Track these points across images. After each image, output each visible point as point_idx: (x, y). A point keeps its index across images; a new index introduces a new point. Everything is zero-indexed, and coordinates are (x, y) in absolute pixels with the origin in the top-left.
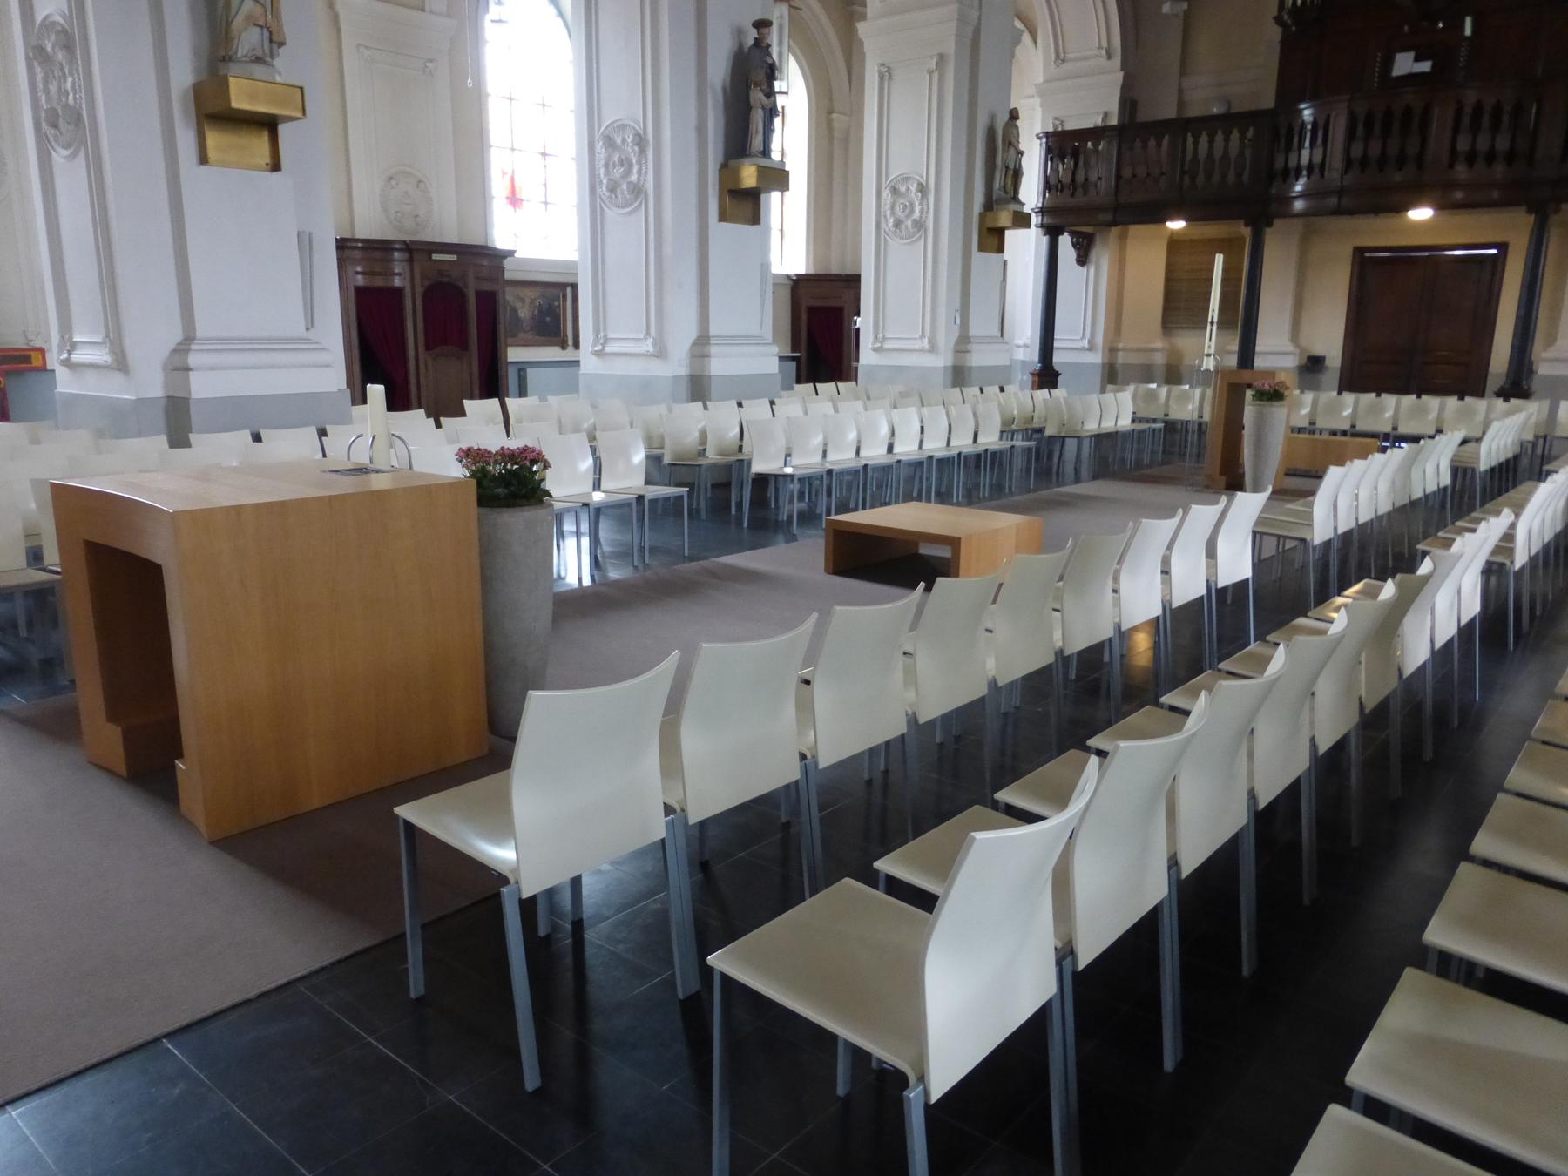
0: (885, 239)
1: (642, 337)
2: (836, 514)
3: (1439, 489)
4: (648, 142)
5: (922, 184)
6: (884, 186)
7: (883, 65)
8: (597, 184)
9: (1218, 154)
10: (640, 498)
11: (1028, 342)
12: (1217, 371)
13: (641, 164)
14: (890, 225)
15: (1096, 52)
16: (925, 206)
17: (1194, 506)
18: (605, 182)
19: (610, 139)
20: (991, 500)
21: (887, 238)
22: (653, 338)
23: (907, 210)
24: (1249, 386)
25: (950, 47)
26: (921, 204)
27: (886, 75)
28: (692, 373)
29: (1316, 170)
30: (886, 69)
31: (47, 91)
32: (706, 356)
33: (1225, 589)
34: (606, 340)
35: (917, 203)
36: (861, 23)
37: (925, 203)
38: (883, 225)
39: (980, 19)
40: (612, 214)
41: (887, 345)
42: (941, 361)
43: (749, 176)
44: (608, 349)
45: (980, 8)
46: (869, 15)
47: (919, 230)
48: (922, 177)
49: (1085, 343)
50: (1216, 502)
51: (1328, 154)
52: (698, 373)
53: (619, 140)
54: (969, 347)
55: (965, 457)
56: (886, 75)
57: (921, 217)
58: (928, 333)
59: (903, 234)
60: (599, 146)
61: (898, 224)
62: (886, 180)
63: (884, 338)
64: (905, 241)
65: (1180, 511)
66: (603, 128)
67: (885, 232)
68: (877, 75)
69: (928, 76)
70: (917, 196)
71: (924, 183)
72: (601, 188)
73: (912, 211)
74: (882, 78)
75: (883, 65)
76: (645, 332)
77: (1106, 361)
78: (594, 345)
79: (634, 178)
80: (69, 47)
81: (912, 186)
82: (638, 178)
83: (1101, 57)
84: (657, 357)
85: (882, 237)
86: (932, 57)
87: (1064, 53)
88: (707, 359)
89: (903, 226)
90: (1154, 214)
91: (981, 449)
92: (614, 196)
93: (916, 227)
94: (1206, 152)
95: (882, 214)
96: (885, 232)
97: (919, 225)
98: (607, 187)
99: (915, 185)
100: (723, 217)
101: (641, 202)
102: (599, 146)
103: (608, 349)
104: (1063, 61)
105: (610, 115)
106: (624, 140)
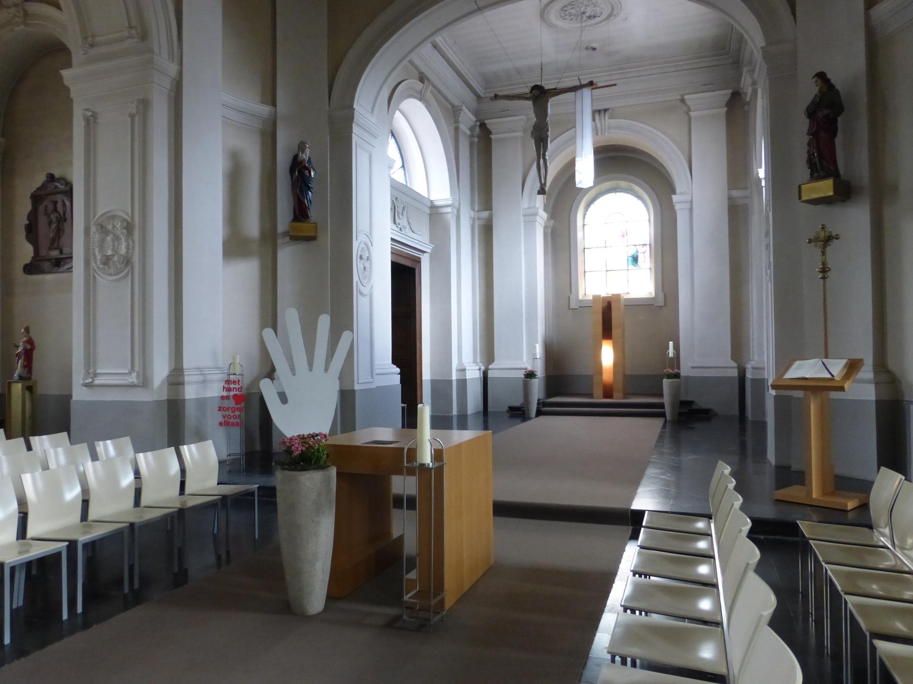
7: (87, 110)
12: (466, 379)
18: (99, 257)
19: (102, 226)
21: (96, 275)
22: (137, 372)
26: (127, 241)
31: (102, 247)
34: (96, 375)
36: (63, 70)
38: (93, 264)
39: (180, 73)
41: (98, 381)
57: (127, 252)
61: (107, 260)
66: (96, 218)
69: (129, 119)
70: (122, 233)
75: (87, 110)
76: (130, 368)
80: (129, 228)
83: (132, 37)
85: (91, 274)
88: (181, 386)
89: (111, 262)
91: (98, 532)
95: (91, 252)
101: (129, 271)
106: (114, 227)
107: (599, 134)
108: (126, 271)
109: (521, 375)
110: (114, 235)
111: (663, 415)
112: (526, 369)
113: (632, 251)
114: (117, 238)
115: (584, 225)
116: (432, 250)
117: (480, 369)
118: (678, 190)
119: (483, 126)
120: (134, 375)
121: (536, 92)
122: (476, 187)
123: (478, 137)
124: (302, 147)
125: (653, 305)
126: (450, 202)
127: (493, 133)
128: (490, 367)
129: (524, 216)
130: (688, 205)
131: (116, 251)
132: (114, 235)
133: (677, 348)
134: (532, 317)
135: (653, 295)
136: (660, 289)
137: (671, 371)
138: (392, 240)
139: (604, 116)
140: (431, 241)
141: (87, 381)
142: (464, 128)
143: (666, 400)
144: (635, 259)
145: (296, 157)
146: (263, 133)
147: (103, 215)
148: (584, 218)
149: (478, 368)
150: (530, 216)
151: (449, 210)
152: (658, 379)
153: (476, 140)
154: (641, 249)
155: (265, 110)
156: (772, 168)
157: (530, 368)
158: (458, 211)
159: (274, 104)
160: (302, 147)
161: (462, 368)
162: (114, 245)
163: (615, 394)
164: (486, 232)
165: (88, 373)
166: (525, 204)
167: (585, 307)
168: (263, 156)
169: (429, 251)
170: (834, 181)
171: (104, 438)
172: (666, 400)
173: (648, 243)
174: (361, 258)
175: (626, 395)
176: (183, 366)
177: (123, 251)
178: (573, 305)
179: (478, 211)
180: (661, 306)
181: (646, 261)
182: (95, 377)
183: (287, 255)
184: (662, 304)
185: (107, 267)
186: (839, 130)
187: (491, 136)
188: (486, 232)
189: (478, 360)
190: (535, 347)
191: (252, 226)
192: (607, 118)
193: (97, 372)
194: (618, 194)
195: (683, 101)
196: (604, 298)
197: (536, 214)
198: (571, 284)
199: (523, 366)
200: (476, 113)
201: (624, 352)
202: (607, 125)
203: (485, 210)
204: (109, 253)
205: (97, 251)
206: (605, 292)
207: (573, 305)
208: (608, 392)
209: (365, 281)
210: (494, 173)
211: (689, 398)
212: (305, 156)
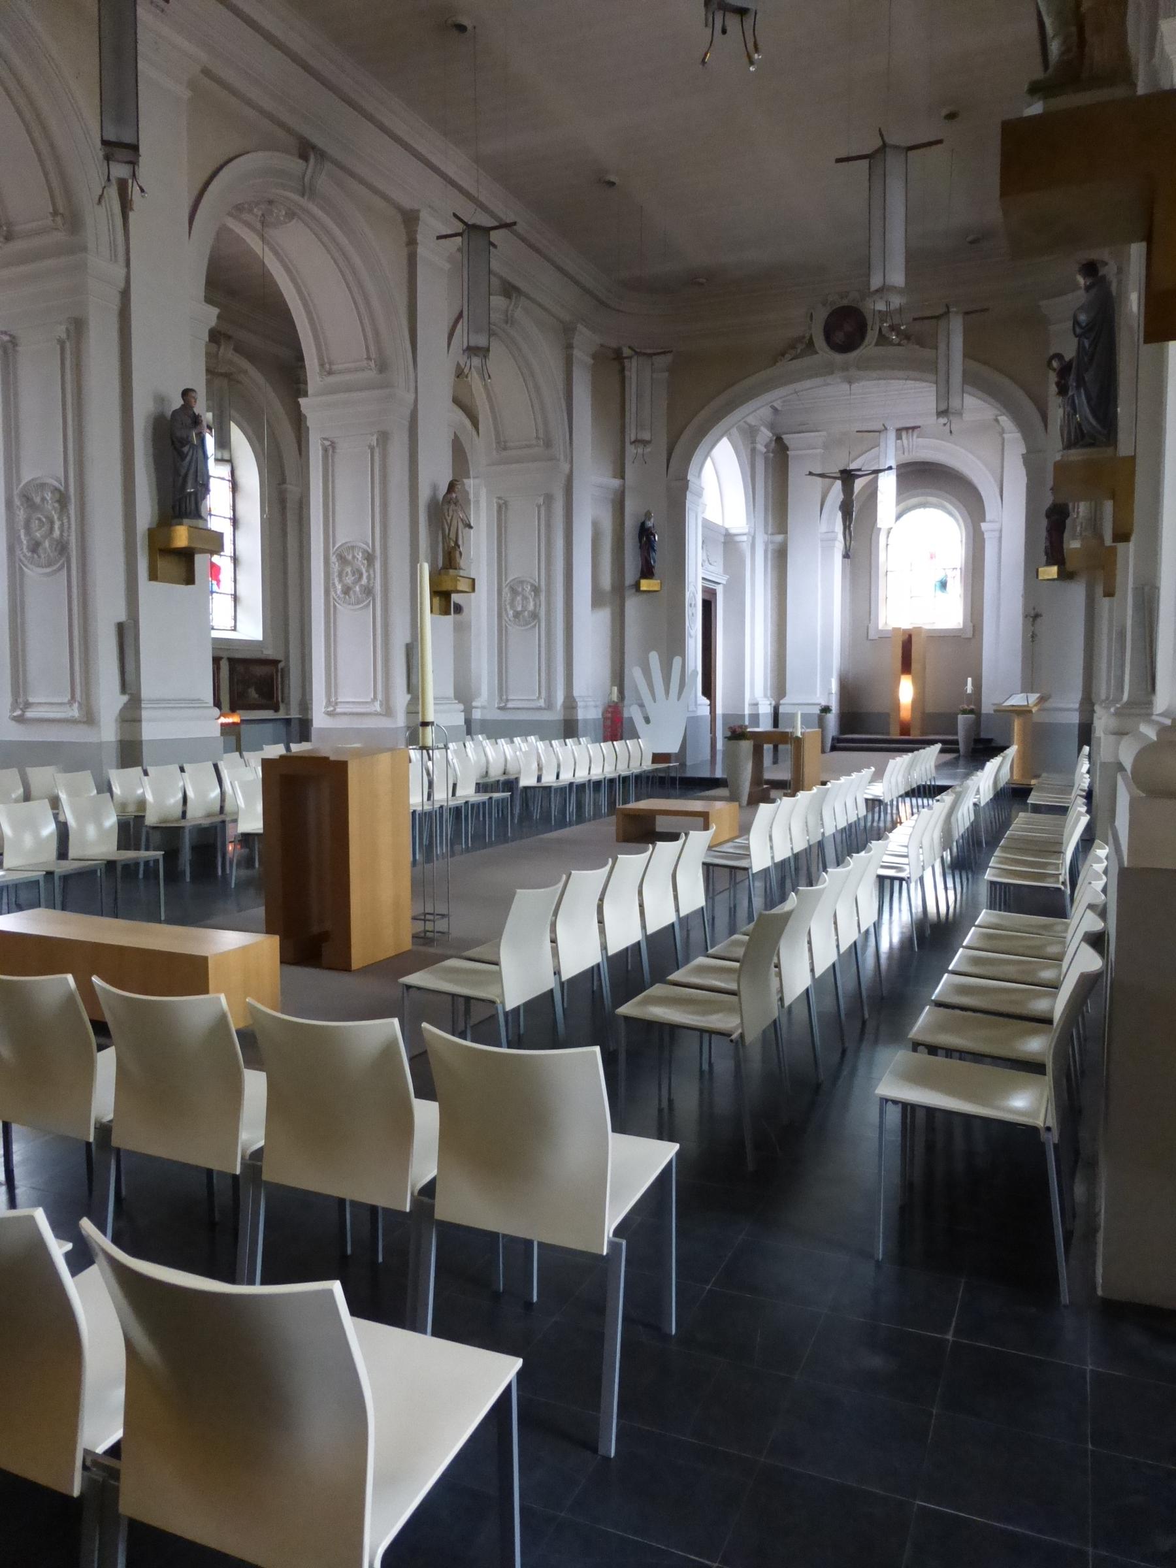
0: (506, 627)
1: (369, 700)
2: (956, 734)
3: (859, 819)
4: (69, 498)
6: (504, 585)
10: (49, 874)
11: (485, 704)
13: (62, 521)
14: (339, 592)
15: (534, 442)
16: (371, 572)
17: (518, 891)
20: (608, 816)
26: (534, 600)
27: (330, 449)
28: (566, 718)
30: (329, 443)
32: (139, 720)
33: (516, 1010)
34: (28, 705)
40: (33, 573)
41: (510, 705)
43: (181, 536)
46: (310, 392)
47: (534, 619)
48: (535, 580)
49: (542, 703)
50: (645, 851)
52: (569, 718)
53: (38, 500)
55: (473, 805)
56: (330, 449)
57: (61, 535)
58: (380, 697)
59: (353, 599)
60: (333, 559)
62: (333, 547)
63: (507, 700)
64: (523, 628)
65: (610, 860)
67: (334, 599)
68: (320, 448)
70: (363, 564)
71: (370, 551)
72: (22, 549)
73: (52, 529)
74: (325, 450)
77: (119, 738)
78: (13, 710)
79: (364, 581)
81: (358, 554)
84: (84, 723)
85: (332, 604)
86: (373, 435)
91: (460, 802)
96: (334, 599)
97: (368, 591)
98: (28, 547)
100: (153, 576)
102: (333, 559)
105: (27, 475)
106: (43, 499)
107: (906, 454)
108: (533, 624)
109: (817, 710)
110: (523, 596)
111: (957, 751)
112: (819, 704)
113: (940, 577)
114: (525, 598)
115: (887, 545)
116: (727, 581)
117: (771, 704)
118: (988, 517)
119: (779, 440)
120: (76, 705)
121: (845, 475)
122: (770, 508)
123: (773, 452)
124: (648, 515)
125: (960, 636)
126: (746, 531)
127: (790, 448)
128: (781, 702)
129: (822, 541)
130: (997, 534)
131: (524, 608)
132: (523, 596)
133: (978, 686)
134: (827, 649)
135: (961, 626)
136: (969, 618)
137: (966, 707)
138: (703, 579)
139: (912, 436)
140: (726, 572)
141: (329, 710)
142: (761, 448)
143: (961, 736)
144: (943, 585)
145: (643, 524)
146: (613, 501)
147: (514, 580)
148: (888, 537)
149: (769, 703)
150: (829, 541)
151: (744, 538)
152: (953, 718)
153: (771, 455)
154: (950, 574)
155: (616, 483)
156: (81, 1376)
157: (824, 703)
158: (754, 538)
159: (623, 478)
160: (648, 515)
161: (755, 702)
162: (523, 604)
163: (912, 732)
164: (780, 558)
165: (17, 702)
166: (823, 528)
167: (885, 638)
168: (614, 523)
169: (724, 582)
170: (1058, 569)
171: (555, 739)
172: (961, 736)
173: (959, 567)
174: (691, 605)
175: (923, 734)
176: (140, 695)
177: (531, 607)
178: (872, 635)
179: (772, 534)
180: (967, 638)
181: (956, 588)
182: (27, 708)
183: (632, 605)
184: (969, 635)
185: (35, 556)
186: (1066, 530)
187: (788, 452)
188: (780, 558)
189: (769, 695)
190: (831, 681)
191: (606, 582)
192: (915, 437)
193: (339, 700)
194: (927, 509)
195: (997, 421)
196: (905, 631)
197: (834, 539)
198: (870, 612)
199: (817, 701)
200: (772, 427)
201: (924, 687)
202: (915, 443)
203: (779, 533)
204: (519, 609)
205: (508, 607)
206: (906, 624)
207: (872, 635)
208: (905, 729)
209: (692, 625)
210: (790, 489)
211: (990, 737)
212: (649, 524)
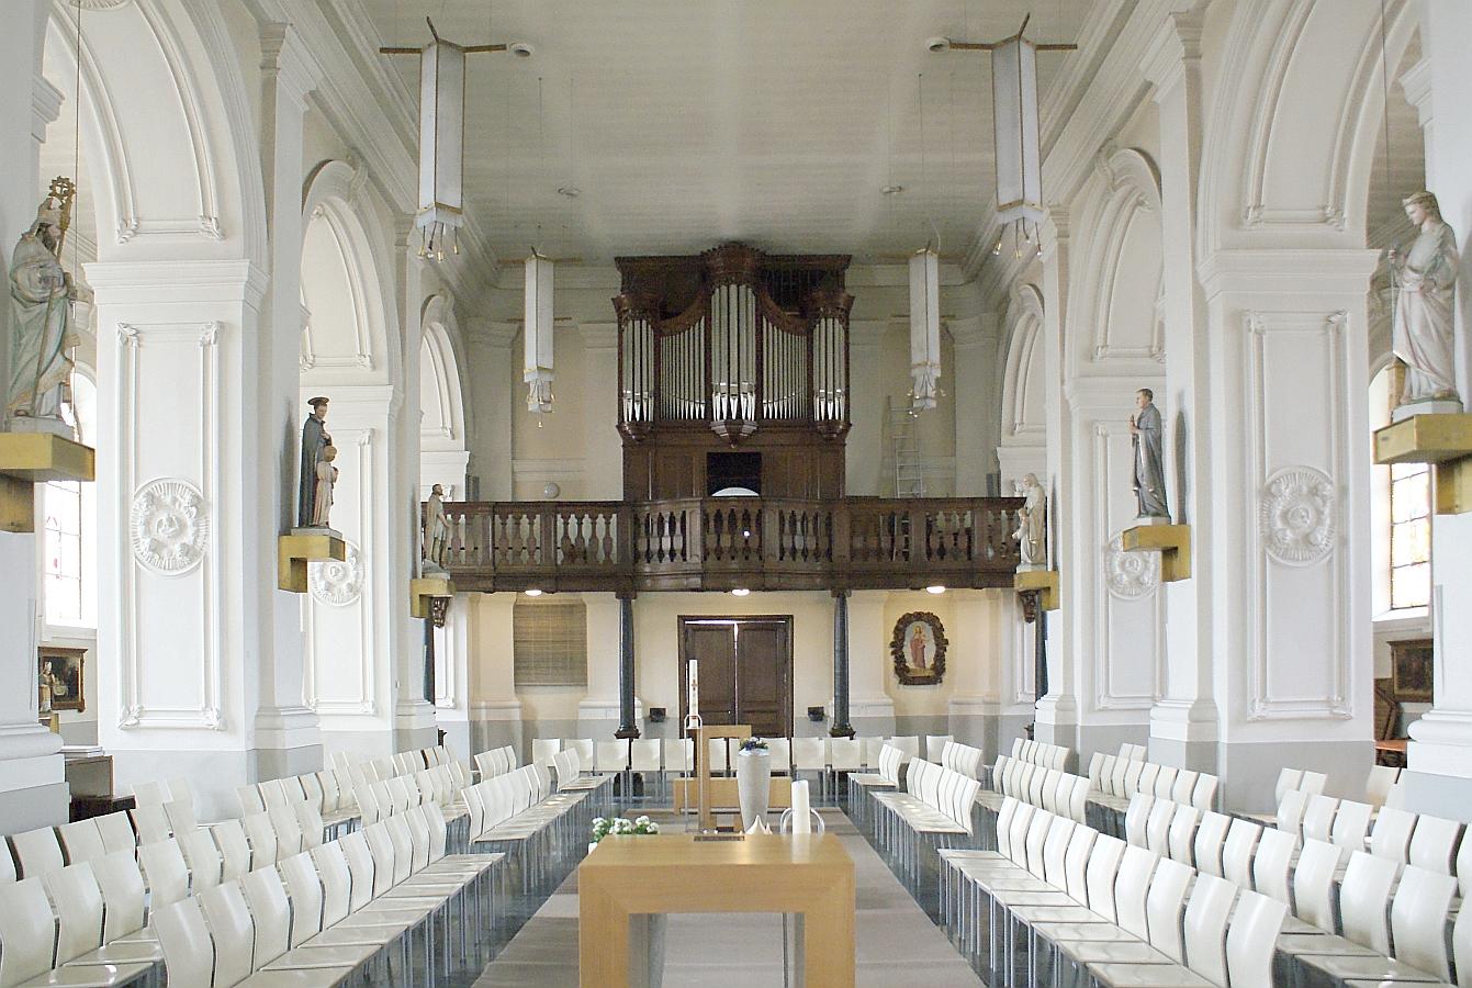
5: (198, 497)
6: (133, 492)
8: (132, 542)
9: (601, 534)
16: (361, 572)
23: (340, 574)
24: (794, 773)
25: (235, 315)
27: (133, 338)
29: (679, 555)
30: (134, 332)
35: (189, 522)
37: (361, 568)
39: (270, 285)
42: (237, 745)
44: (144, 723)
45: (271, 272)
51: (688, 542)
54: (278, 722)
61: (156, 547)
82: (195, 541)
87: (138, 219)
89: (165, 553)
90: (517, 582)
92: (157, 557)
93: (187, 554)
94: (604, 534)
99: (188, 497)
103: (144, 723)
104: (135, 233)
